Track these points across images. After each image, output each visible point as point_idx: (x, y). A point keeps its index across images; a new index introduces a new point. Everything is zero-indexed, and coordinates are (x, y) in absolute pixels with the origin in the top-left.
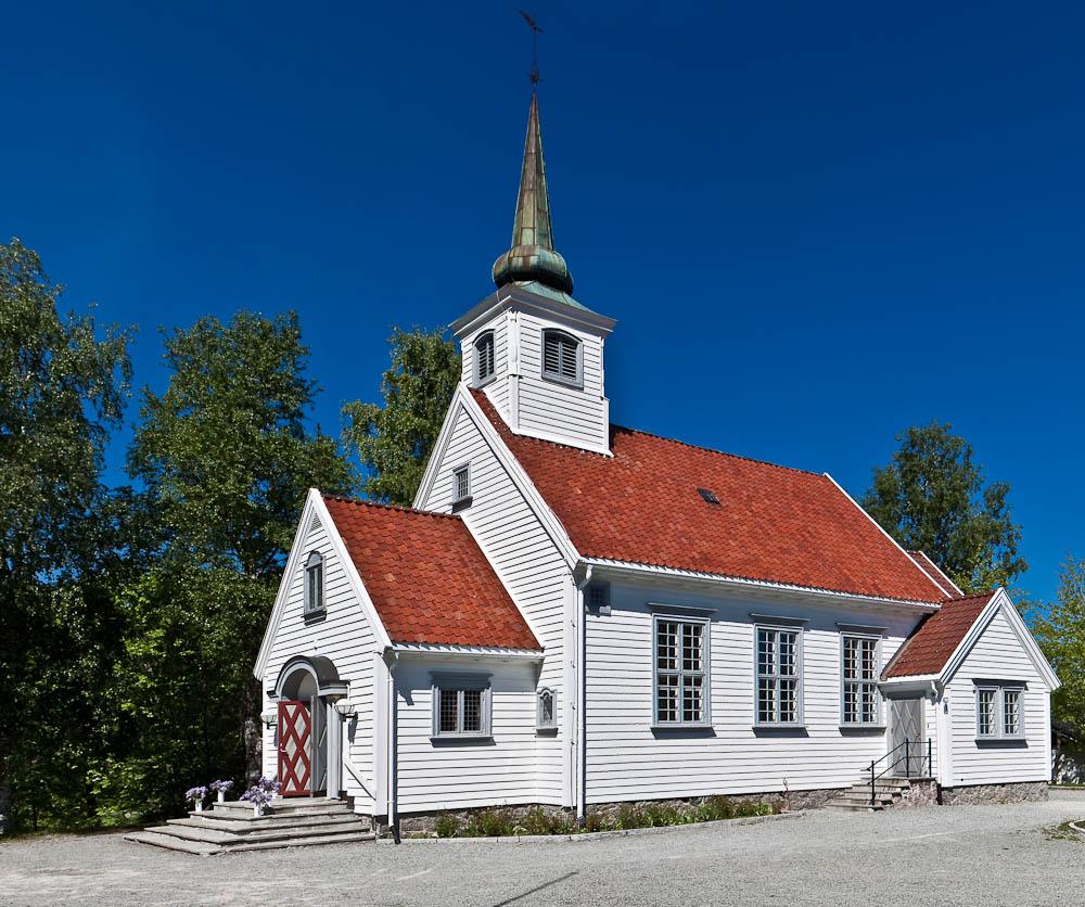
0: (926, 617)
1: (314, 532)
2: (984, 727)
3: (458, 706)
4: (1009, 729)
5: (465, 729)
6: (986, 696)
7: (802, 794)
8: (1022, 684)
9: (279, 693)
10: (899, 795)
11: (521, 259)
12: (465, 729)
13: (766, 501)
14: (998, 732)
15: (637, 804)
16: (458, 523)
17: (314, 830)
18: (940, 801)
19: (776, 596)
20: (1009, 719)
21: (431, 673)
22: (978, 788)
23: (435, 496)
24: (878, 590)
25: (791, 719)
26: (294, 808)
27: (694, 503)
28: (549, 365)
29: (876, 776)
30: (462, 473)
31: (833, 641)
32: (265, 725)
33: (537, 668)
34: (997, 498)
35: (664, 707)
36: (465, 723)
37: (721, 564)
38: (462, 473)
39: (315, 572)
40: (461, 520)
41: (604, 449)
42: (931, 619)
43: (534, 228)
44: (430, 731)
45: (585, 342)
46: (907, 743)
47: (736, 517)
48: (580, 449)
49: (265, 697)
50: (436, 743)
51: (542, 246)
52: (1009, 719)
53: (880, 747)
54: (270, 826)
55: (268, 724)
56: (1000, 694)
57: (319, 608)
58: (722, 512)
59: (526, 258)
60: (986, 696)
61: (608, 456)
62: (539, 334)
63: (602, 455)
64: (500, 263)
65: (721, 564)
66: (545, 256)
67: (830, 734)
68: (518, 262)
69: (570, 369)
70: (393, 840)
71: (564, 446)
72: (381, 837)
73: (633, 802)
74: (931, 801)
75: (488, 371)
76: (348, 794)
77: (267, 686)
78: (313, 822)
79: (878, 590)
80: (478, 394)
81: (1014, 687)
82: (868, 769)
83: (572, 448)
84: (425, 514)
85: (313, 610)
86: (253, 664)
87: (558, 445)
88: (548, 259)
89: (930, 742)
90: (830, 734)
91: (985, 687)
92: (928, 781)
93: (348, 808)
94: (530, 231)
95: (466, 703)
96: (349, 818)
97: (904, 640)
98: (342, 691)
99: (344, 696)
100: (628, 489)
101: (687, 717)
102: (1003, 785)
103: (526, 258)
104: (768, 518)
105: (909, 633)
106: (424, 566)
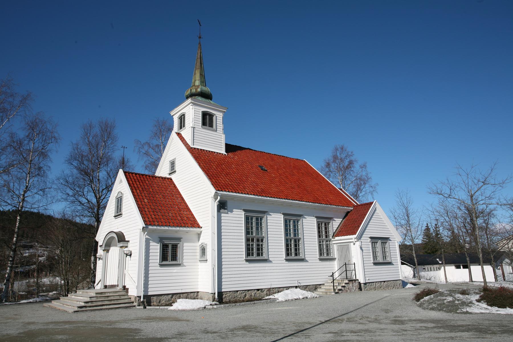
0: (348, 213)
1: (120, 185)
2: (375, 257)
3: (169, 253)
4: (385, 257)
5: (172, 260)
6: (384, 244)
7: (305, 287)
8: (387, 239)
9: (104, 246)
10: (344, 287)
11: (195, 90)
12: (172, 260)
13: (284, 169)
14: (380, 259)
15: (239, 292)
16: (170, 181)
17: (113, 302)
18: (360, 289)
19: (291, 205)
20: (384, 252)
21: (159, 238)
22: (375, 283)
23: (162, 171)
24: (329, 202)
25: (291, 255)
26: (106, 292)
27: (257, 170)
28: (204, 124)
29: (334, 279)
30: (173, 164)
31: (280, 218)
32: (98, 259)
33: (199, 235)
34: (364, 166)
35: (249, 252)
36: (172, 258)
37: (270, 193)
38: (173, 164)
39: (119, 201)
40: (171, 179)
41: (223, 151)
42: (350, 213)
43: (199, 80)
44: (158, 261)
45: (217, 115)
46: (346, 264)
47: (274, 176)
48: (215, 152)
49: (99, 248)
50: (161, 265)
51: (202, 85)
52: (384, 252)
53: (335, 266)
54: (96, 300)
55: (99, 258)
56: (379, 242)
57: (119, 213)
58: (268, 174)
59: (196, 89)
60: (384, 244)
61: (225, 154)
62: (201, 113)
63: (223, 154)
64: (187, 91)
65: (270, 193)
66: (203, 88)
67: (314, 261)
68: (194, 91)
69: (211, 125)
70: (142, 307)
71: (209, 151)
72: (138, 306)
73: (237, 291)
74: (357, 289)
75: (183, 126)
76: (126, 287)
77: (100, 243)
78: (112, 299)
79: (329, 202)
80: (179, 134)
81: (385, 240)
82: (331, 276)
83: (212, 152)
84: (159, 177)
85: (118, 214)
86: (95, 237)
87: (207, 151)
88: (204, 89)
89: (354, 264)
90: (314, 261)
91: (374, 240)
92: (355, 280)
93: (126, 293)
94: (198, 81)
95: (172, 250)
96: (126, 297)
97: (341, 220)
98: (126, 245)
99: (127, 247)
100: (233, 166)
101: (258, 255)
102: (384, 282)
103: (196, 89)
104: (285, 176)
105: (343, 218)
106: (158, 196)
